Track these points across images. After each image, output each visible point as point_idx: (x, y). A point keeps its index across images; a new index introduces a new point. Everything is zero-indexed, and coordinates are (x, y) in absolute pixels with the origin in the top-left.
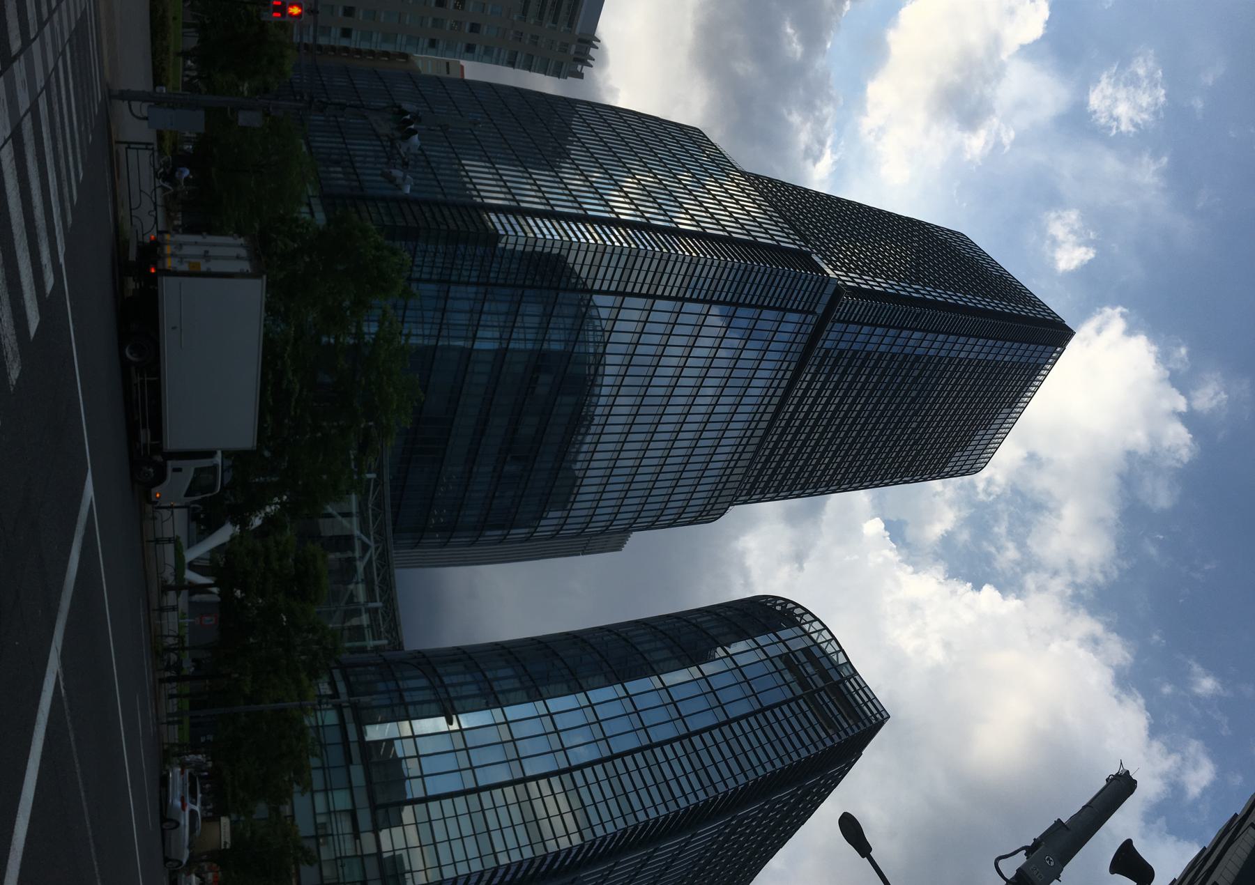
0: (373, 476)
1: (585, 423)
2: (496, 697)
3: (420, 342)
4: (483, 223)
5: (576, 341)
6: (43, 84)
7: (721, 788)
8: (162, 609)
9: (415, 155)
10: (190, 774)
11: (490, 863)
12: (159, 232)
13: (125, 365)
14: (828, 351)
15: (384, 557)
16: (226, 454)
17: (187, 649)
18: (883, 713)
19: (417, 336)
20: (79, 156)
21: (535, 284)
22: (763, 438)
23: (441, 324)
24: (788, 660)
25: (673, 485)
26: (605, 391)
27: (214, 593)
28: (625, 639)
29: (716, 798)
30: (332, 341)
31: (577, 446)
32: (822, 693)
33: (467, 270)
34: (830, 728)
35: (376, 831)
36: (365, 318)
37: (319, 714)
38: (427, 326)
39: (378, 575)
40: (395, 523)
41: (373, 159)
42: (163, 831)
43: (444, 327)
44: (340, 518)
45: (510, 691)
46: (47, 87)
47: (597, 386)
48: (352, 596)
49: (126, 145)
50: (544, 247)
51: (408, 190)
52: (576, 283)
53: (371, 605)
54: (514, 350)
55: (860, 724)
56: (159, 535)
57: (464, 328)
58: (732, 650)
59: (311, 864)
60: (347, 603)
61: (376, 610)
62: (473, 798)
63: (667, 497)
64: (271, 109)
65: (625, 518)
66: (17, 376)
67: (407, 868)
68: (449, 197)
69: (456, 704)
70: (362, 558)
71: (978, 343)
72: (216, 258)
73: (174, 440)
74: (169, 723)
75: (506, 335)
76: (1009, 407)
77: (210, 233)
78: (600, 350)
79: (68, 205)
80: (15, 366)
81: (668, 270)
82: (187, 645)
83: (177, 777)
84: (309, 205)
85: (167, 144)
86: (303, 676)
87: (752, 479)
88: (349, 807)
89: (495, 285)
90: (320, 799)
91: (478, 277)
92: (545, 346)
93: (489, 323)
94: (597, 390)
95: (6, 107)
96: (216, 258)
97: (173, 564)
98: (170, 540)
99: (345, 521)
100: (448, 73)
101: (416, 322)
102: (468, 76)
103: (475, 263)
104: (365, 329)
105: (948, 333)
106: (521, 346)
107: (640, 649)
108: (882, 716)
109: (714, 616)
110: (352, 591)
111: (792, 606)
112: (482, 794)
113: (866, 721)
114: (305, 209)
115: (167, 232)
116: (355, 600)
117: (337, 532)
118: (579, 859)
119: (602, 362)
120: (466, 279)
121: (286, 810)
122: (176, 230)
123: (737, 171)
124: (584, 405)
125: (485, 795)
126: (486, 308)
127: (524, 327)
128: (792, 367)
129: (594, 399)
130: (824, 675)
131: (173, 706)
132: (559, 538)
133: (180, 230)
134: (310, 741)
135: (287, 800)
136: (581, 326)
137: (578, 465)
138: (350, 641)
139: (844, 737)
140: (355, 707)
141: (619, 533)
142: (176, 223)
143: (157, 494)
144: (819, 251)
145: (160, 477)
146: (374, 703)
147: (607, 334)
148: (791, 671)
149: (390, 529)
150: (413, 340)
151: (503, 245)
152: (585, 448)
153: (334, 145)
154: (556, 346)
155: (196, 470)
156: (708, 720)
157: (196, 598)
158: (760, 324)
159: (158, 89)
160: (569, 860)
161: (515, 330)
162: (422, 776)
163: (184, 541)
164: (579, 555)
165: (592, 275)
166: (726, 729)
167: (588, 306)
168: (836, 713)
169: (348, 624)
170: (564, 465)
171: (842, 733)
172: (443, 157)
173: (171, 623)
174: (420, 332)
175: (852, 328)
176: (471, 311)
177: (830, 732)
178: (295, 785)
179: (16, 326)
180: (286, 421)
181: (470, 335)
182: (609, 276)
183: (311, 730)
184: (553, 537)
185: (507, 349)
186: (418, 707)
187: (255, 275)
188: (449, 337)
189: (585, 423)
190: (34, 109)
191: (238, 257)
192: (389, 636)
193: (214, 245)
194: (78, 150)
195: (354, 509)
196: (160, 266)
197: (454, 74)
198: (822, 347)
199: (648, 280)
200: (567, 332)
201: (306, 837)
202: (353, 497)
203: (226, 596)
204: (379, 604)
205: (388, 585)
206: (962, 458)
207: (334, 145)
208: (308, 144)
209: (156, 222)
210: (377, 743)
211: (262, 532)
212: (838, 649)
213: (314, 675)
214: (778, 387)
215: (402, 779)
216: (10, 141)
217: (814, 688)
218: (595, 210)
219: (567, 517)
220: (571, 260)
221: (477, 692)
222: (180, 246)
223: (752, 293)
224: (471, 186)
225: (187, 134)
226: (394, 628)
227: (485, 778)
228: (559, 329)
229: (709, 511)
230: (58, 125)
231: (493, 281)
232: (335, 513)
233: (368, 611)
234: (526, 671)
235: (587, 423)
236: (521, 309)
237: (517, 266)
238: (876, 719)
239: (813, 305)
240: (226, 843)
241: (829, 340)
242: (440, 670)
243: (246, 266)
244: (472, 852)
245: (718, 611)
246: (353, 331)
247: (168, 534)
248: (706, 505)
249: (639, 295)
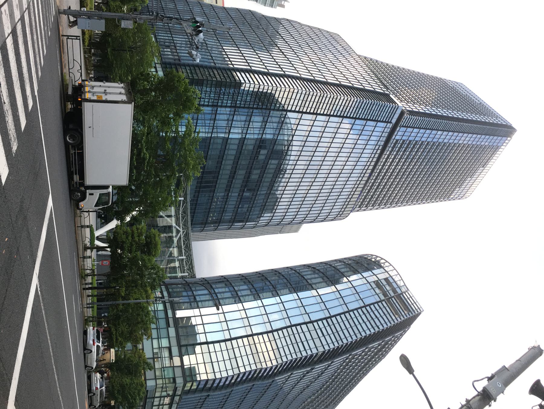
0: (182, 199)
1: (282, 173)
2: (239, 298)
3: (204, 135)
4: (233, 77)
5: (279, 134)
6: (26, 7)
7: (345, 341)
8: (84, 258)
9: (202, 43)
10: (97, 330)
11: (236, 371)
12: (83, 80)
13: (66, 144)
14: (397, 140)
15: (187, 236)
16: (114, 187)
17: (96, 275)
18: (421, 309)
19: (203, 132)
20: (44, 42)
21: (259, 107)
22: (367, 181)
23: (213, 126)
24: (378, 284)
26: (292, 158)
27: (108, 251)
28: (298, 273)
29: (342, 345)
30: (164, 134)
31: (278, 183)
32: (393, 299)
33: (226, 100)
34: (397, 314)
35: (181, 356)
36: (180, 124)
37: (155, 305)
38: (207, 128)
39: (184, 244)
40: (192, 221)
41: (184, 45)
42: (85, 354)
43: (215, 127)
44: (166, 218)
45: (246, 295)
46: (28, 8)
47: (289, 155)
48: (171, 254)
49: (67, 37)
50: (263, 89)
51: (198, 61)
52: (279, 107)
53: (180, 258)
54: (248, 139)
55: (410, 313)
56: (83, 224)
57: (225, 128)
58: (351, 278)
59: (150, 370)
60: (169, 257)
61: (183, 259)
62: (228, 343)
63: (321, 208)
64: (137, 19)
65: (300, 217)
66: (16, 148)
67: (197, 372)
68: (217, 65)
69: (221, 301)
70: (176, 236)
71: (468, 136)
72: (110, 93)
73: (90, 181)
74: (87, 308)
75: (245, 131)
76: (483, 167)
77: (107, 81)
78: (290, 139)
79: (39, 67)
80: (15, 144)
82: (96, 273)
83: (91, 331)
84: (155, 68)
85: (87, 36)
86: (148, 289)
87: (361, 200)
88: (168, 345)
89: (240, 107)
90: (155, 342)
91: (231, 103)
92: (264, 136)
93: (237, 126)
94: (288, 158)
95: (9, 18)
96: (110, 93)
97: (89, 237)
98: (88, 227)
99: (168, 219)
100: (217, 3)
101: (202, 126)
103: (207, 95)
104: (180, 129)
105: (454, 132)
106: (252, 136)
107: (306, 278)
108: (420, 310)
109: (343, 263)
110: (171, 251)
112: (233, 341)
113: (413, 312)
114: (153, 70)
115: (86, 80)
116: (173, 255)
117: (165, 224)
118: (275, 371)
119: (291, 144)
120: (225, 104)
121: (140, 346)
122: (91, 79)
123: (357, 55)
124: (282, 164)
125: (234, 342)
126: (235, 118)
127: (253, 128)
128: (380, 148)
129: (287, 162)
130: (394, 291)
131: (89, 300)
132: (269, 226)
133: (93, 80)
134: (151, 317)
135: (141, 342)
136: (281, 127)
137: (279, 192)
138: (170, 273)
139: (403, 319)
140: (172, 304)
141: (297, 224)
142: (91, 76)
143: (82, 204)
144: (394, 93)
145: (83, 198)
146: (181, 301)
147: (294, 131)
148: (379, 288)
149: (189, 223)
150: (201, 135)
151: (244, 88)
152: (282, 184)
153: (167, 38)
154: (269, 137)
155: (100, 194)
156: (339, 310)
157: (100, 253)
158: (366, 128)
159: (82, 9)
160: (271, 372)
161: (249, 129)
162: (205, 333)
163: (94, 227)
164: (278, 233)
165: (287, 103)
166: (347, 315)
167: (285, 118)
168: (399, 308)
169: (169, 266)
170: (272, 192)
171: (402, 317)
172: (214, 45)
173: (88, 263)
174: (204, 131)
175: (422, 131)
176: (228, 120)
177: (397, 316)
178: (144, 336)
179: (15, 126)
180: (142, 173)
181: (227, 131)
182: (295, 104)
183: (152, 312)
184: (266, 225)
185: (245, 138)
186: (203, 303)
187: (129, 102)
188: (217, 132)
189: (282, 173)
190: (22, 19)
191: (120, 93)
192: (189, 272)
193: (109, 87)
194: (44, 40)
195: (173, 214)
196: (83, 97)
198: (394, 139)
199: (299, 104)
200: (274, 130)
201: (148, 358)
202: (173, 208)
203: (114, 252)
204: (184, 257)
205: (188, 248)
206: (459, 191)
207: (167, 38)
208: (155, 37)
209: (81, 76)
210: (182, 318)
211: (130, 224)
212: (400, 279)
213: (153, 288)
214: (374, 157)
215: (195, 334)
216: (11, 35)
217: (390, 296)
218: (290, 71)
219: (273, 216)
220: (277, 96)
221: (231, 296)
222: (93, 87)
223: (382, 112)
224: (228, 59)
225: (97, 32)
226: (191, 268)
227: (234, 334)
228: (271, 128)
229: (341, 215)
230: (34, 27)
231: (238, 105)
232: (164, 215)
233: (179, 260)
234: (253, 287)
235: (283, 173)
236: (252, 119)
237: (250, 98)
238: (418, 311)
239: (391, 119)
240: (112, 360)
241: (398, 135)
242: (214, 286)
243: (124, 98)
244: (229, 367)
245: (344, 261)
246: (174, 130)
247: (87, 223)
248: (340, 212)
249: (336, 116)
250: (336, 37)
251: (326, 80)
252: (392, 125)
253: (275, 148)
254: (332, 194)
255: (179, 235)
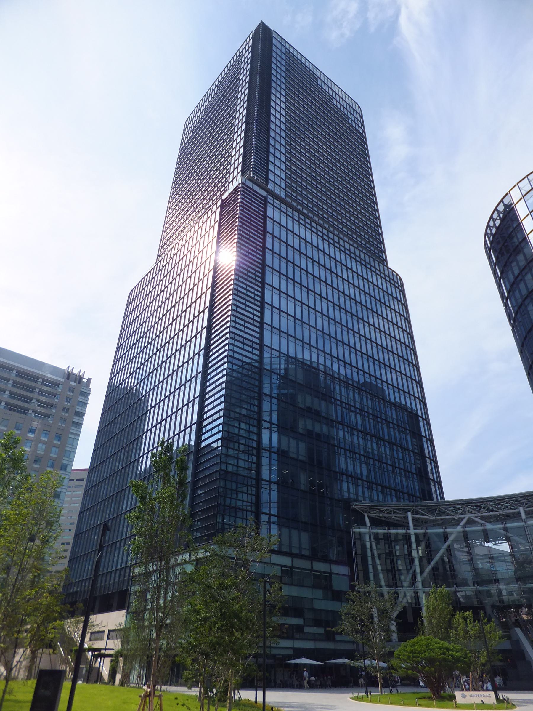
0: (409, 514)
25: (328, 337)
81: (246, 347)
94: (315, 365)
102: (87, 465)
111: (496, 213)
119: (302, 360)
197: (85, 476)
199: (250, 349)
232: (445, 546)
250: (133, 295)
251: (207, 309)
252: (269, 196)
253: (302, 383)
254: (344, 323)
255: (477, 519)
